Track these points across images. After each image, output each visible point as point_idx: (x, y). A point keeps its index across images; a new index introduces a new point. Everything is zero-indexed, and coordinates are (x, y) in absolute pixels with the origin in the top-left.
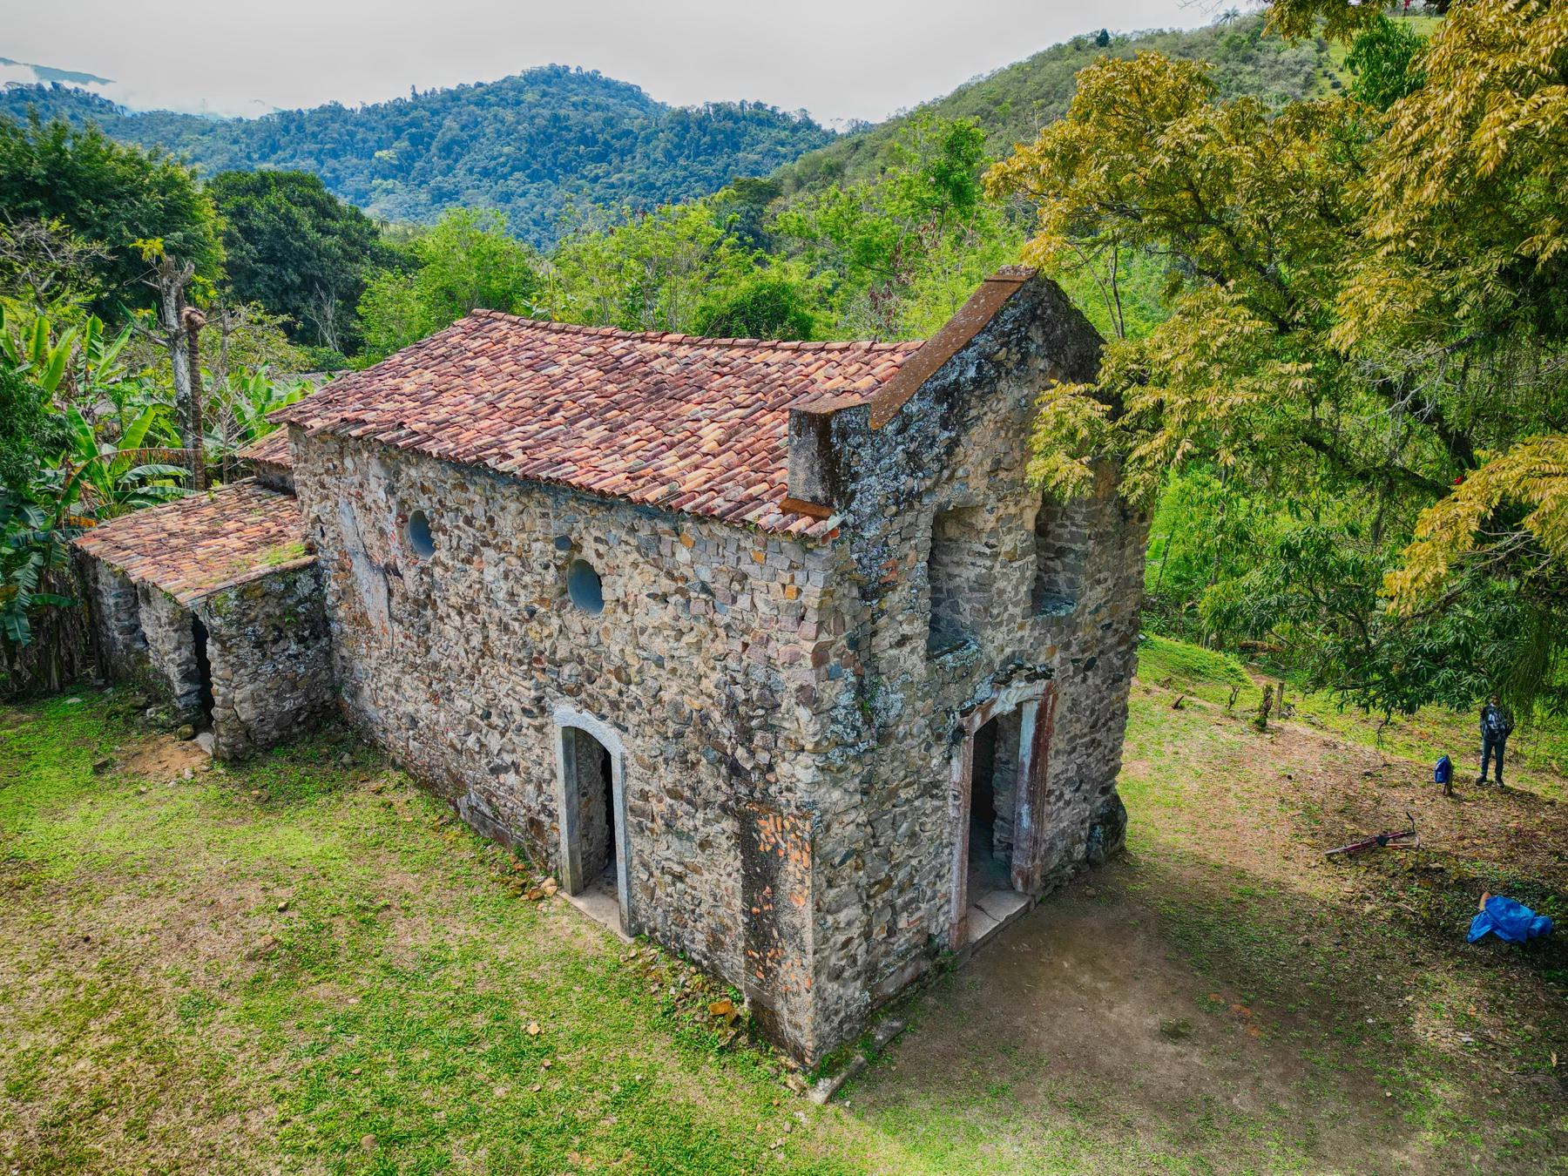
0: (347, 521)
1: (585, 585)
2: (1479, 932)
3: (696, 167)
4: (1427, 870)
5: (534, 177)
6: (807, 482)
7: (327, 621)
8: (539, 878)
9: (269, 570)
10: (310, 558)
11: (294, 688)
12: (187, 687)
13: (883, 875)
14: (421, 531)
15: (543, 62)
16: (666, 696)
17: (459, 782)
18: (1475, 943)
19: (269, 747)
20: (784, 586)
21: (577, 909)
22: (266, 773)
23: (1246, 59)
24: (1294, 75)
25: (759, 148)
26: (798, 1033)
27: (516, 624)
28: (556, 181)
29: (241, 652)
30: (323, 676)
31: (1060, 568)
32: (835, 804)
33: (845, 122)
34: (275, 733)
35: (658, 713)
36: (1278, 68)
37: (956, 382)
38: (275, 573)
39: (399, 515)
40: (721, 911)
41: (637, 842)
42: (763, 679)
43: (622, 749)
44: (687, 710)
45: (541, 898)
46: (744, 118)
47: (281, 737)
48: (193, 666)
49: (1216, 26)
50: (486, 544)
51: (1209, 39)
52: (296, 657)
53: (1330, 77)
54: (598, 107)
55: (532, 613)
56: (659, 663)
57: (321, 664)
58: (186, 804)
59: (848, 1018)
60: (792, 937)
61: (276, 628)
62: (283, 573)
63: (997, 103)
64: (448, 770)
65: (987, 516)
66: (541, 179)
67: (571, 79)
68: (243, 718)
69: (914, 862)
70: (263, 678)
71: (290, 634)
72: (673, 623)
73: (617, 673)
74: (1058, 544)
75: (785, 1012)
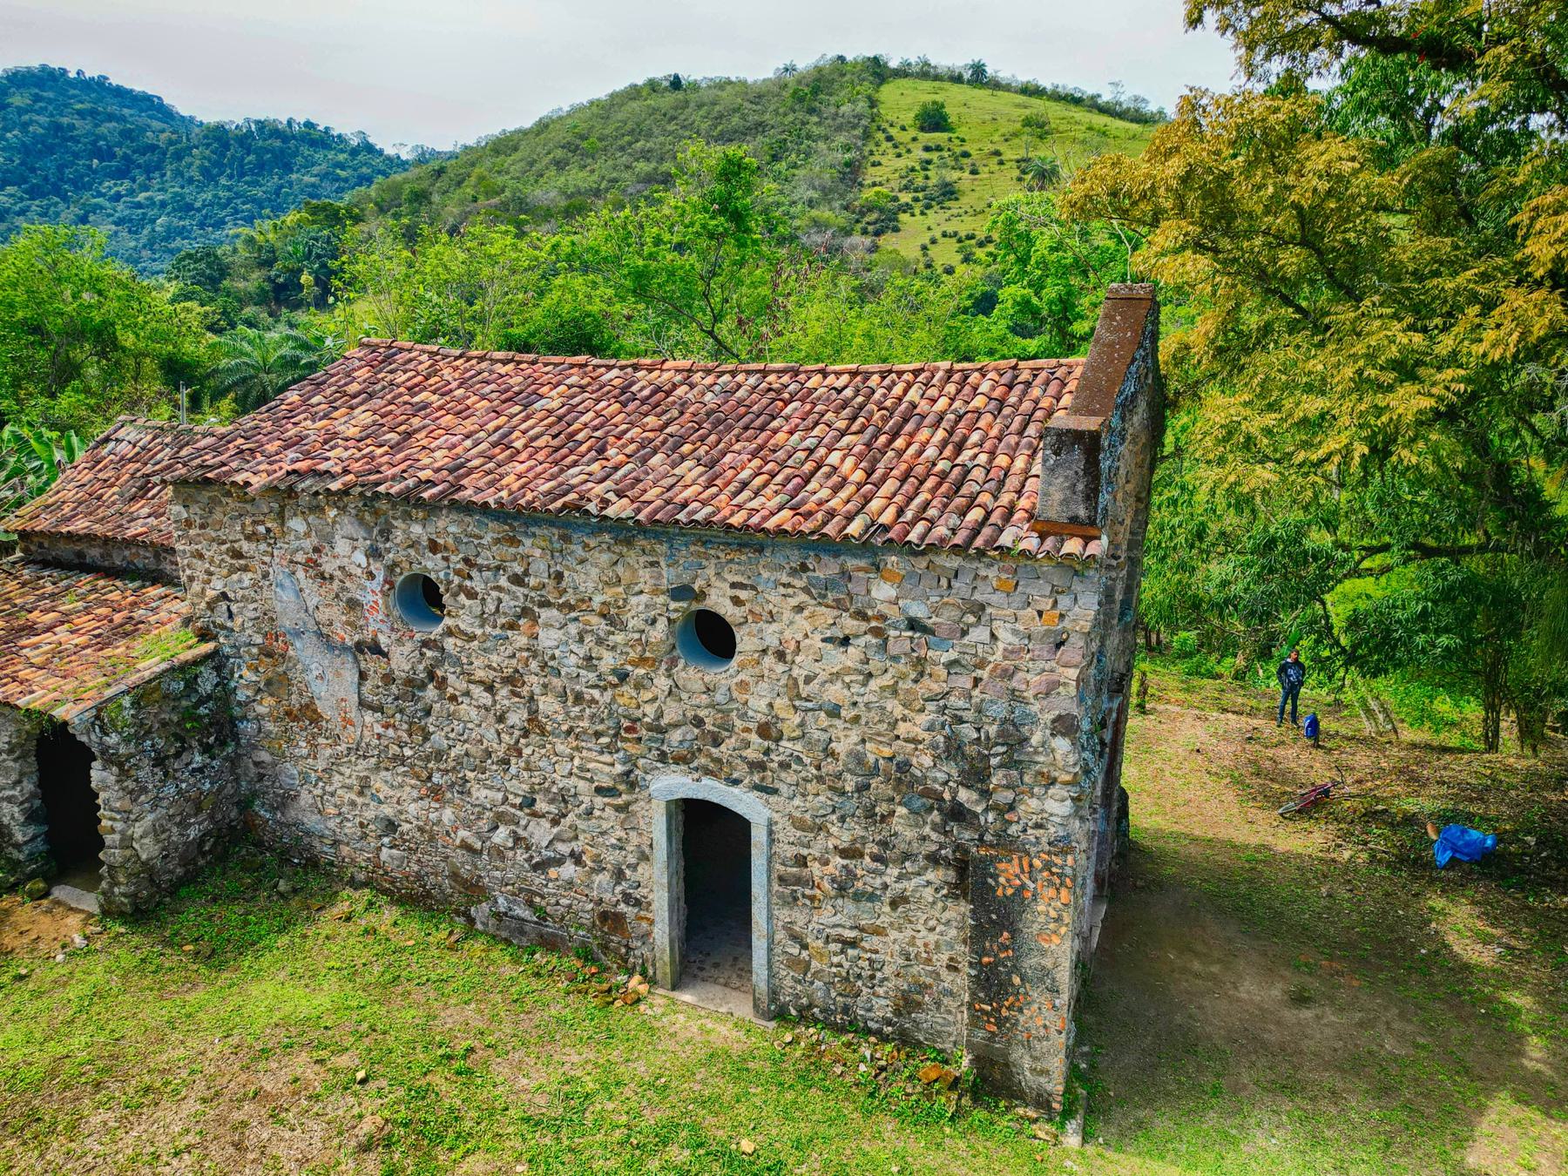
0: (288, 596)
1: (712, 637)
2: (1444, 858)
3: (242, 187)
4: (1376, 812)
5: (34, 193)
6: (1065, 502)
7: (233, 721)
8: (622, 978)
9: (164, 666)
10: (209, 647)
11: (198, 809)
12: (31, 831)
14: (423, 598)
15: (33, 61)
16: (840, 748)
17: (474, 890)
18: (1444, 868)
20: (1040, 613)
21: (688, 1004)
22: (190, 916)
23: (811, 111)
24: (854, 127)
25: (315, 170)
26: (1042, 1080)
27: (596, 693)
28: (65, 199)
29: (141, 774)
33: (409, 148)
35: (829, 767)
36: (839, 120)
38: (172, 669)
39: (386, 581)
40: (915, 970)
41: (784, 915)
42: (1004, 714)
43: (767, 813)
44: (871, 759)
45: (638, 1000)
46: (294, 137)
48: (37, 803)
49: (779, 78)
50: (545, 604)
51: (776, 89)
52: (201, 770)
53: (884, 131)
54: (111, 117)
55: (623, 677)
56: (834, 712)
57: (226, 776)
58: (98, 976)
60: (1041, 980)
62: (183, 667)
63: (583, 138)
64: (455, 876)
66: (43, 195)
67: (72, 84)
68: (144, 857)
70: (165, 803)
72: (859, 666)
73: (764, 731)
75: (1027, 1063)
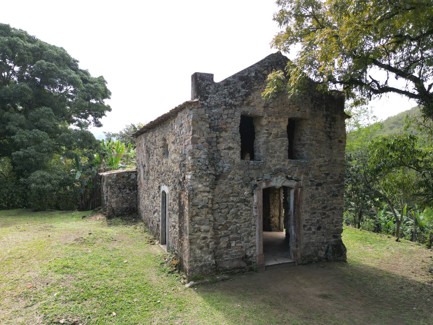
11: (127, 202)
13: (223, 223)
19: (118, 216)
30: (135, 200)
31: (304, 150)
32: (200, 188)
34: (120, 213)
37: (247, 76)
47: (122, 214)
57: (134, 197)
59: (205, 266)
61: (124, 185)
63: (400, 120)
65: (264, 120)
69: (238, 225)
71: (127, 188)
74: (303, 143)
